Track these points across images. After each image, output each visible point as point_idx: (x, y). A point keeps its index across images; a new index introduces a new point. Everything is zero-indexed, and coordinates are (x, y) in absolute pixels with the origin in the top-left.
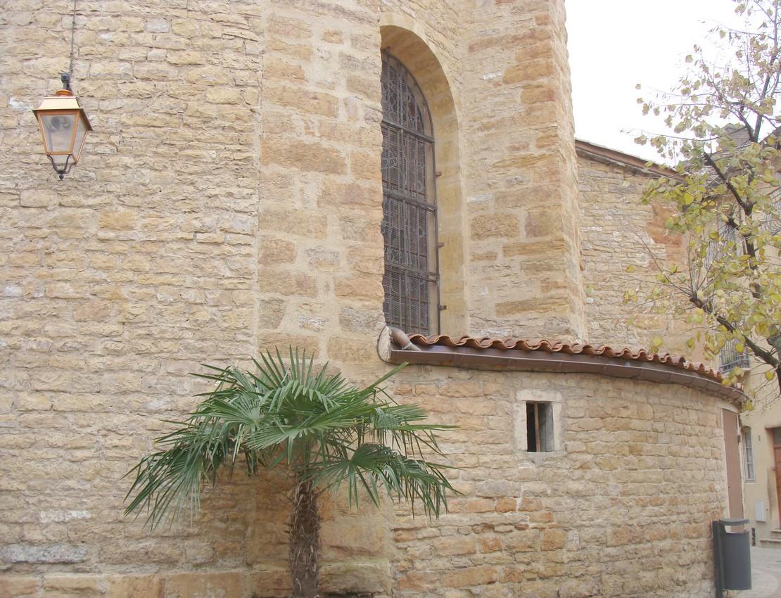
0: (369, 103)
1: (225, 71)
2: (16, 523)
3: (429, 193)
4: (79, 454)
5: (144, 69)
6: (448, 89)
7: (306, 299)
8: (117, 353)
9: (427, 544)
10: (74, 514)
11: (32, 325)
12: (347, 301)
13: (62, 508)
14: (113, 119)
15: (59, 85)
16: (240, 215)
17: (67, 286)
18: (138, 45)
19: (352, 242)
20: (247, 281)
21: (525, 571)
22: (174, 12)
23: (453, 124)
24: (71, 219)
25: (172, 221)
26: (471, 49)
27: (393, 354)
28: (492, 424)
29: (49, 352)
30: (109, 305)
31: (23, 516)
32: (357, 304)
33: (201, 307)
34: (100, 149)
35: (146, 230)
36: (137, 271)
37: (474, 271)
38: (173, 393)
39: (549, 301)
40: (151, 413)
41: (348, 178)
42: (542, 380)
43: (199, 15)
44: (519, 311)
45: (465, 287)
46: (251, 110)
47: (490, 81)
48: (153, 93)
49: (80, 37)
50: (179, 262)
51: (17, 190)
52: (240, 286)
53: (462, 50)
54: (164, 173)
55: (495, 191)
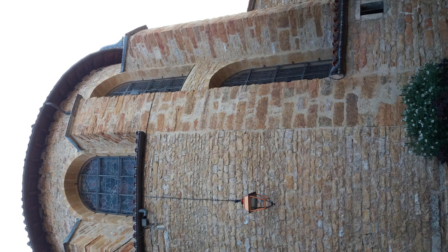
0: (240, 90)
1: (231, 144)
2: (421, 225)
3: (272, 69)
4: (389, 198)
5: (232, 174)
6: (231, 64)
7: (319, 109)
8: (344, 182)
9: (428, 51)
10: (416, 200)
11: (334, 216)
12: (319, 93)
13: (414, 206)
14: (251, 185)
15: (239, 204)
16: (285, 136)
17: (317, 202)
18: (223, 176)
19: (295, 93)
20: (312, 132)
21: (442, 7)
22: (210, 164)
23: (244, 62)
24: (290, 201)
25: (289, 161)
26: (215, 57)
27: (341, 73)
28: (371, 29)
29: (345, 210)
30: (324, 185)
31: (418, 222)
32: (320, 89)
33: (323, 150)
34: (262, 189)
35: (293, 171)
36: (310, 175)
37: (303, 48)
38: (361, 160)
39: (316, 14)
40: (370, 168)
41: (269, 96)
42: (351, 10)
43: (211, 154)
44: (320, 27)
45: (310, 51)
46: (245, 133)
47: (227, 48)
48: (240, 170)
49: (221, 198)
50: (305, 158)
51: (279, 221)
52: (314, 134)
53: (216, 61)
54: (270, 165)
55: (270, 42)
